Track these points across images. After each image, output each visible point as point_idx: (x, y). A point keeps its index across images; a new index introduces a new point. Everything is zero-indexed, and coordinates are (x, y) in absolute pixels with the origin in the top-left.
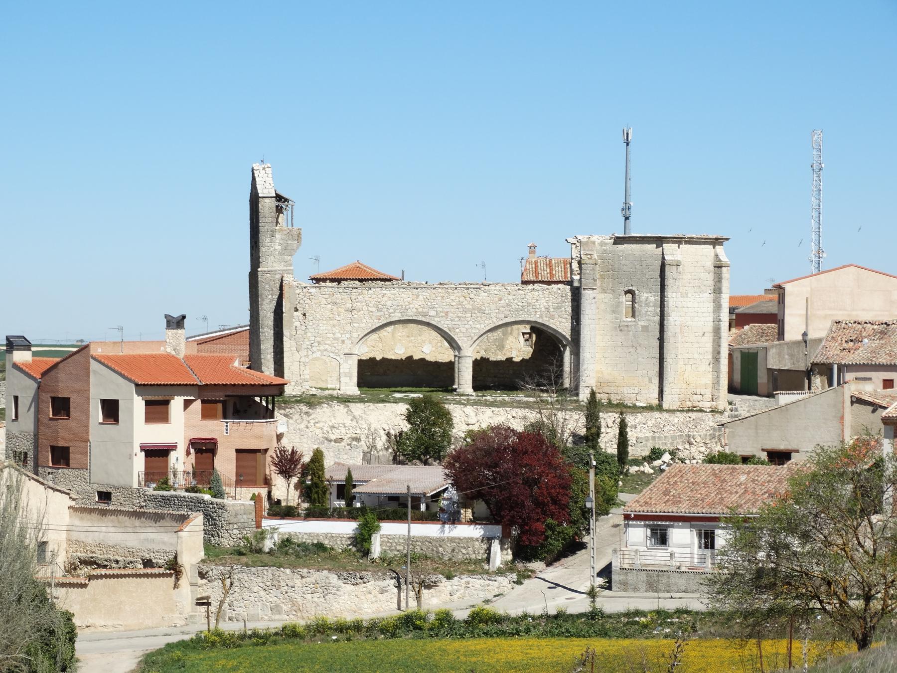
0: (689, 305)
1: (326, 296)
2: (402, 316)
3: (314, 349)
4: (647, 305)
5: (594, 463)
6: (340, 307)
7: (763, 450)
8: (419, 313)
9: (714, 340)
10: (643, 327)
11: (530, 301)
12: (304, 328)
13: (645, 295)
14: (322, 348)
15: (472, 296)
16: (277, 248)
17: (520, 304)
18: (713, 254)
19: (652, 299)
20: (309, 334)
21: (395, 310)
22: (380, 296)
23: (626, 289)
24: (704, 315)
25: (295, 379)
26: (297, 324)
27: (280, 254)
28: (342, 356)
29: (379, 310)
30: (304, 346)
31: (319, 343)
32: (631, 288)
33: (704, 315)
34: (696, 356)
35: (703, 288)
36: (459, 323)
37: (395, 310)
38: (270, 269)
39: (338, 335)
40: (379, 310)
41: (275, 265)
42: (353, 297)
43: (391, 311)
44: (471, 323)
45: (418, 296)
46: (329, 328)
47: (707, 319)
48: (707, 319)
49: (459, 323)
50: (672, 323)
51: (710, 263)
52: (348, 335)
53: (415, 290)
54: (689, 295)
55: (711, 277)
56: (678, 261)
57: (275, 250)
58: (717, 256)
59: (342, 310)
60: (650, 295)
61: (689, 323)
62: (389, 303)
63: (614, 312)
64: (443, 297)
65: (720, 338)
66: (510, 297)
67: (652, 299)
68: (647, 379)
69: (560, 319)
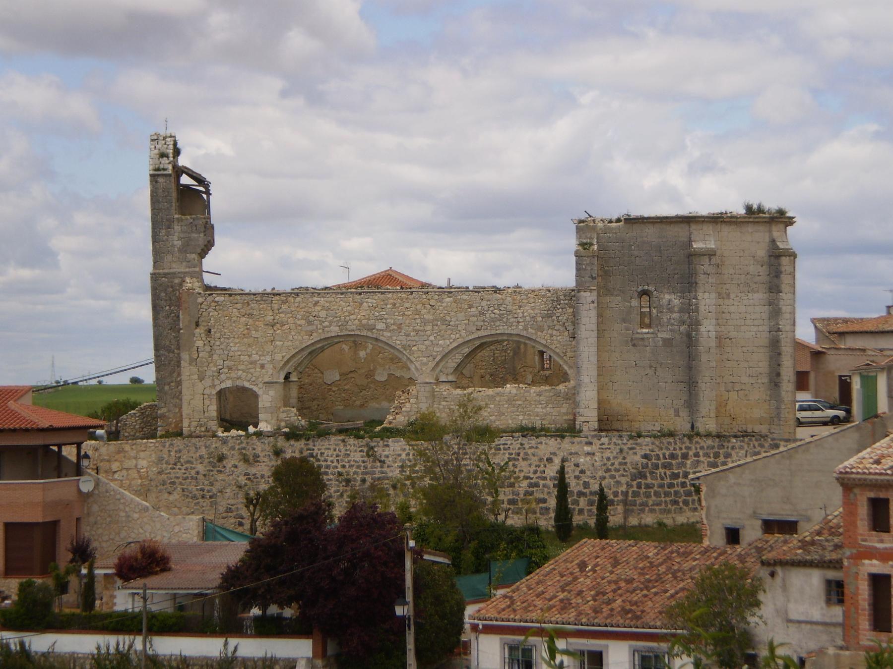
0: (733, 309)
1: (239, 306)
2: (341, 331)
3: (223, 376)
4: (671, 310)
5: (412, 543)
6: (258, 320)
7: (755, 515)
8: (364, 326)
9: (771, 358)
10: (664, 340)
11: (510, 308)
12: (208, 348)
13: (667, 296)
14: (233, 375)
15: (432, 302)
16: (176, 243)
17: (496, 311)
18: (767, 239)
19: (676, 302)
20: (215, 357)
21: (331, 323)
22: (310, 305)
23: (640, 288)
24: (756, 322)
25: (197, 417)
26: (200, 343)
27: (180, 250)
28: (261, 385)
29: (310, 323)
30: (209, 373)
31: (230, 369)
32: (646, 287)
33: (756, 322)
34: (745, 379)
35: (754, 286)
36: (416, 338)
37: (331, 323)
38: (166, 271)
39: (255, 357)
40: (310, 323)
41: (174, 265)
42: (276, 307)
43: (326, 324)
44: (432, 338)
45: (361, 304)
46: (243, 348)
47: (761, 328)
48: (761, 328)
49: (416, 338)
50: (705, 334)
51: (762, 252)
52: (268, 358)
53: (358, 297)
54: (732, 296)
55: (763, 270)
56: (712, 250)
57: (173, 246)
58: (773, 241)
59: (261, 324)
60: (673, 297)
61: (733, 334)
62: (323, 314)
63: (624, 320)
64: (394, 305)
65: (780, 354)
66: (484, 303)
67: (676, 302)
68: (672, 411)
69: (550, 331)
